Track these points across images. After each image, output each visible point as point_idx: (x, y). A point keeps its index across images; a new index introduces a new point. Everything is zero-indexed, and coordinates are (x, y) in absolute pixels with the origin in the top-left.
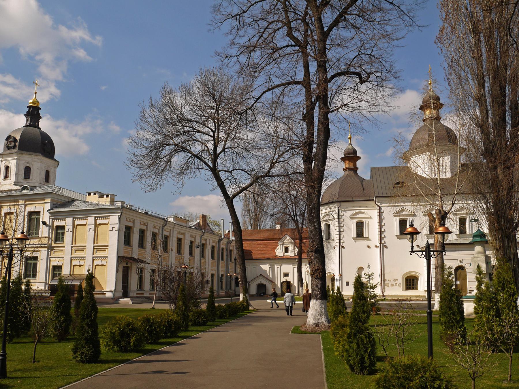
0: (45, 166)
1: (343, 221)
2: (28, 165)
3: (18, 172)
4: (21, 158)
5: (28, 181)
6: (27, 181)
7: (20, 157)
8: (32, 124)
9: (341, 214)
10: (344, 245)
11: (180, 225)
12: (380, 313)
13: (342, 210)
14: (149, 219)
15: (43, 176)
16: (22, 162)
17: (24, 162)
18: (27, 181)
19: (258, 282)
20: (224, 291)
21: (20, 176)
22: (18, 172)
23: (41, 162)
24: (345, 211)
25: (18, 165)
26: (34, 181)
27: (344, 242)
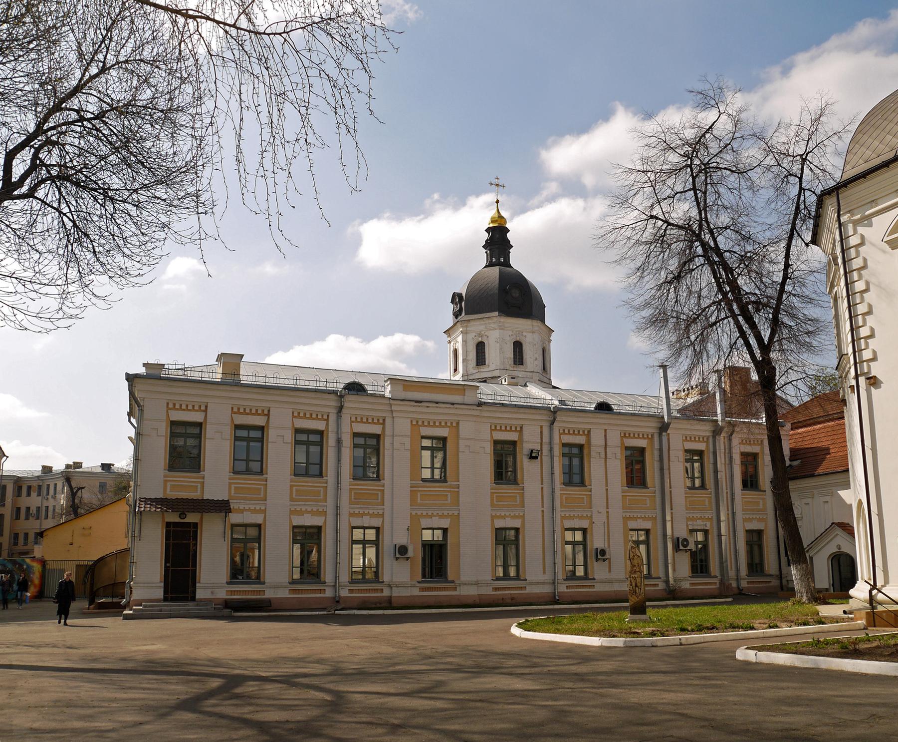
0: (510, 333)
1: (865, 267)
2: (480, 339)
3: (466, 357)
4: (468, 329)
5: (521, 368)
6: (482, 370)
7: (467, 327)
8: (494, 260)
9: (854, 241)
10: (876, 370)
11: (453, 404)
12: (328, 697)
13: (856, 223)
14: (269, 398)
15: (509, 353)
16: (471, 336)
17: (474, 334)
18: (482, 370)
19: (832, 549)
20: (716, 581)
21: (470, 362)
22: (466, 357)
23: (501, 328)
24: (866, 220)
25: (465, 341)
26: (492, 367)
27: (874, 359)
